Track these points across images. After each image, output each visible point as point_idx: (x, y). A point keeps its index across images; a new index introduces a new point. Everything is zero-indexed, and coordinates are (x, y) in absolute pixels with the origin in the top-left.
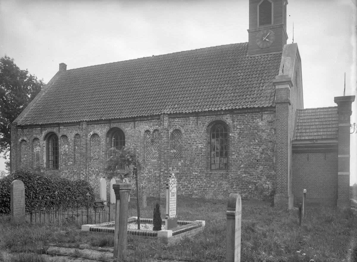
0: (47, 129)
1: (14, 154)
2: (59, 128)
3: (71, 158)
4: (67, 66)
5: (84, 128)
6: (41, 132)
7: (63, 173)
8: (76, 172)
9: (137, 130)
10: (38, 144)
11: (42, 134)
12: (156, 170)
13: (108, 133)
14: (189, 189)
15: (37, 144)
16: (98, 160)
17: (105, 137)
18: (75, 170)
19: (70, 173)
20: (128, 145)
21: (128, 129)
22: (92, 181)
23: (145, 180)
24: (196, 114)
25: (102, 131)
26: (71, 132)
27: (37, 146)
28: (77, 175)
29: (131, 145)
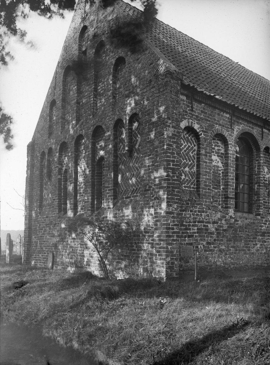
10: (216, 148)
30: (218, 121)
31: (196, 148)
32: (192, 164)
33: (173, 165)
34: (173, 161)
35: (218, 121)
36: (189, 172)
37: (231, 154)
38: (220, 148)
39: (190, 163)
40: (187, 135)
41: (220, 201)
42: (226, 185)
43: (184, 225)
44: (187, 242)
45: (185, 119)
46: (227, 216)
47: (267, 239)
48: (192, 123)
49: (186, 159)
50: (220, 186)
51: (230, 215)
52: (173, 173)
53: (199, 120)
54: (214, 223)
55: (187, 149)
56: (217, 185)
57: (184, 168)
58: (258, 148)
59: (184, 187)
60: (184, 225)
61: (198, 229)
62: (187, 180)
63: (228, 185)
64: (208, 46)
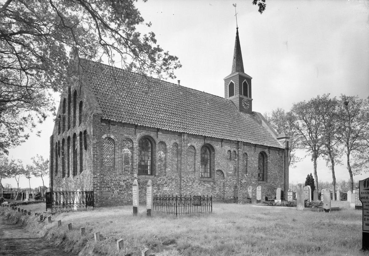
0: (142, 132)
1: (98, 152)
2: (157, 134)
3: (169, 165)
4: (252, 80)
5: (185, 140)
6: (135, 134)
7: (161, 179)
8: (174, 178)
9: (223, 149)
10: (127, 145)
11: (137, 135)
12: (234, 180)
13: (203, 147)
14: (157, 183)
15: (126, 145)
16: (191, 169)
17: (200, 150)
18: (173, 177)
19: (168, 179)
20: (217, 159)
21: (217, 147)
22: (189, 187)
23: (228, 187)
24: (256, 146)
25: (198, 144)
26: (169, 140)
27: (125, 147)
28: (175, 181)
29: (219, 159)
30: (126, 132)
31: (113, 146)
32: (111, 154)
33: (97, 156)
34: (97, 154)
35: (126, 132)
36: (110, 158)
37: (135, 147)
38: (130, 145)
39: (110, 154)
40: (108, 141)
41: (129, 170)
42: (133, 162)
43: (105, 183)
44: (107, 190)
45: (105, 134)
46: (133, 177)
47: (161, 188)
48: (109, 135)
49: (107, 152)
50: (129, 163)
51: (135, 177)
52: (96, 160)
53: (114, 133)
54: (124, 181)
55: (108, 147)
56: (127, 163)
57: (107, 156)
58: (155, 143)
59: (107, 165)
60: (105, 183)
61: (113, 184)
62: (108, 162)
63: (133, 162)
64: (170, 82)
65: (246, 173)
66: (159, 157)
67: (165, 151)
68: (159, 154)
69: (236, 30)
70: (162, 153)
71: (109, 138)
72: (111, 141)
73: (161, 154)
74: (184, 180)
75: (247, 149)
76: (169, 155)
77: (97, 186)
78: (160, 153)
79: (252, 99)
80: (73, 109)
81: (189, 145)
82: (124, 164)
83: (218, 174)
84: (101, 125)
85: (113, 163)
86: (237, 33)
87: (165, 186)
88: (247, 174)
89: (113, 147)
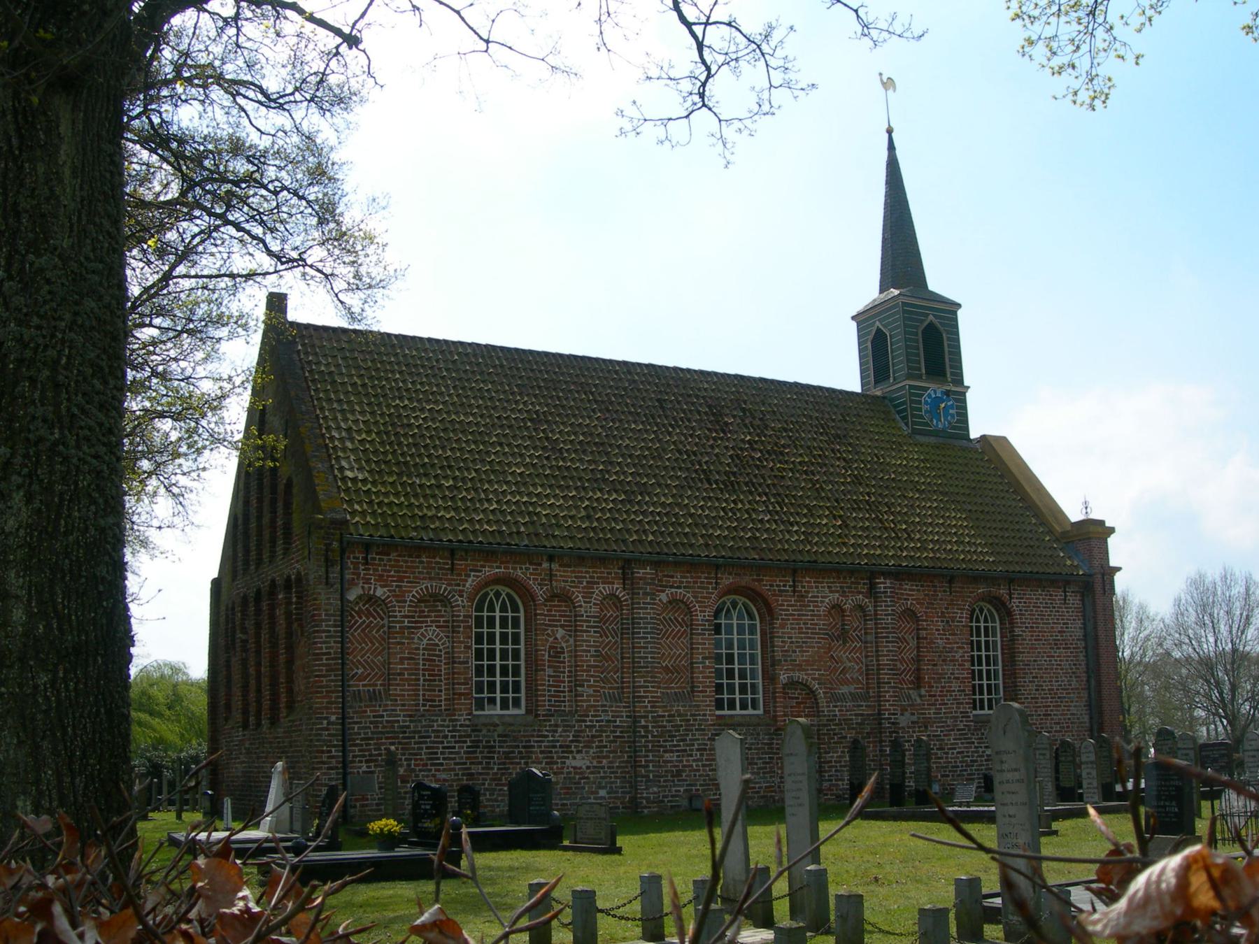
4: (960, 313)
30: (427, 573)
35: (427, 573)
65: (919, 687)
66: (551, 647)
67: (574, 629)
68: (551, 639)
69: (886, 135)
70: (561, 633)
71: (370, 599)
72: (378, 606)
73: (556, 639)
74: (647, 727)
75: (912, 594)
76: (590, 638)
77: (328, 757)
78: (554, 634)
79: (968, 387)
80: (223, 590)
81: (664, 597)
82: (424, 680)
83: (793, 698)
84: (822, 412)
85: (384, 680)
86: (891, 147)
87: (572, 752)
88: (923, 692)
89: (383, 626)
